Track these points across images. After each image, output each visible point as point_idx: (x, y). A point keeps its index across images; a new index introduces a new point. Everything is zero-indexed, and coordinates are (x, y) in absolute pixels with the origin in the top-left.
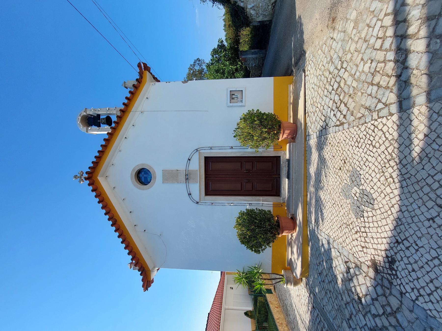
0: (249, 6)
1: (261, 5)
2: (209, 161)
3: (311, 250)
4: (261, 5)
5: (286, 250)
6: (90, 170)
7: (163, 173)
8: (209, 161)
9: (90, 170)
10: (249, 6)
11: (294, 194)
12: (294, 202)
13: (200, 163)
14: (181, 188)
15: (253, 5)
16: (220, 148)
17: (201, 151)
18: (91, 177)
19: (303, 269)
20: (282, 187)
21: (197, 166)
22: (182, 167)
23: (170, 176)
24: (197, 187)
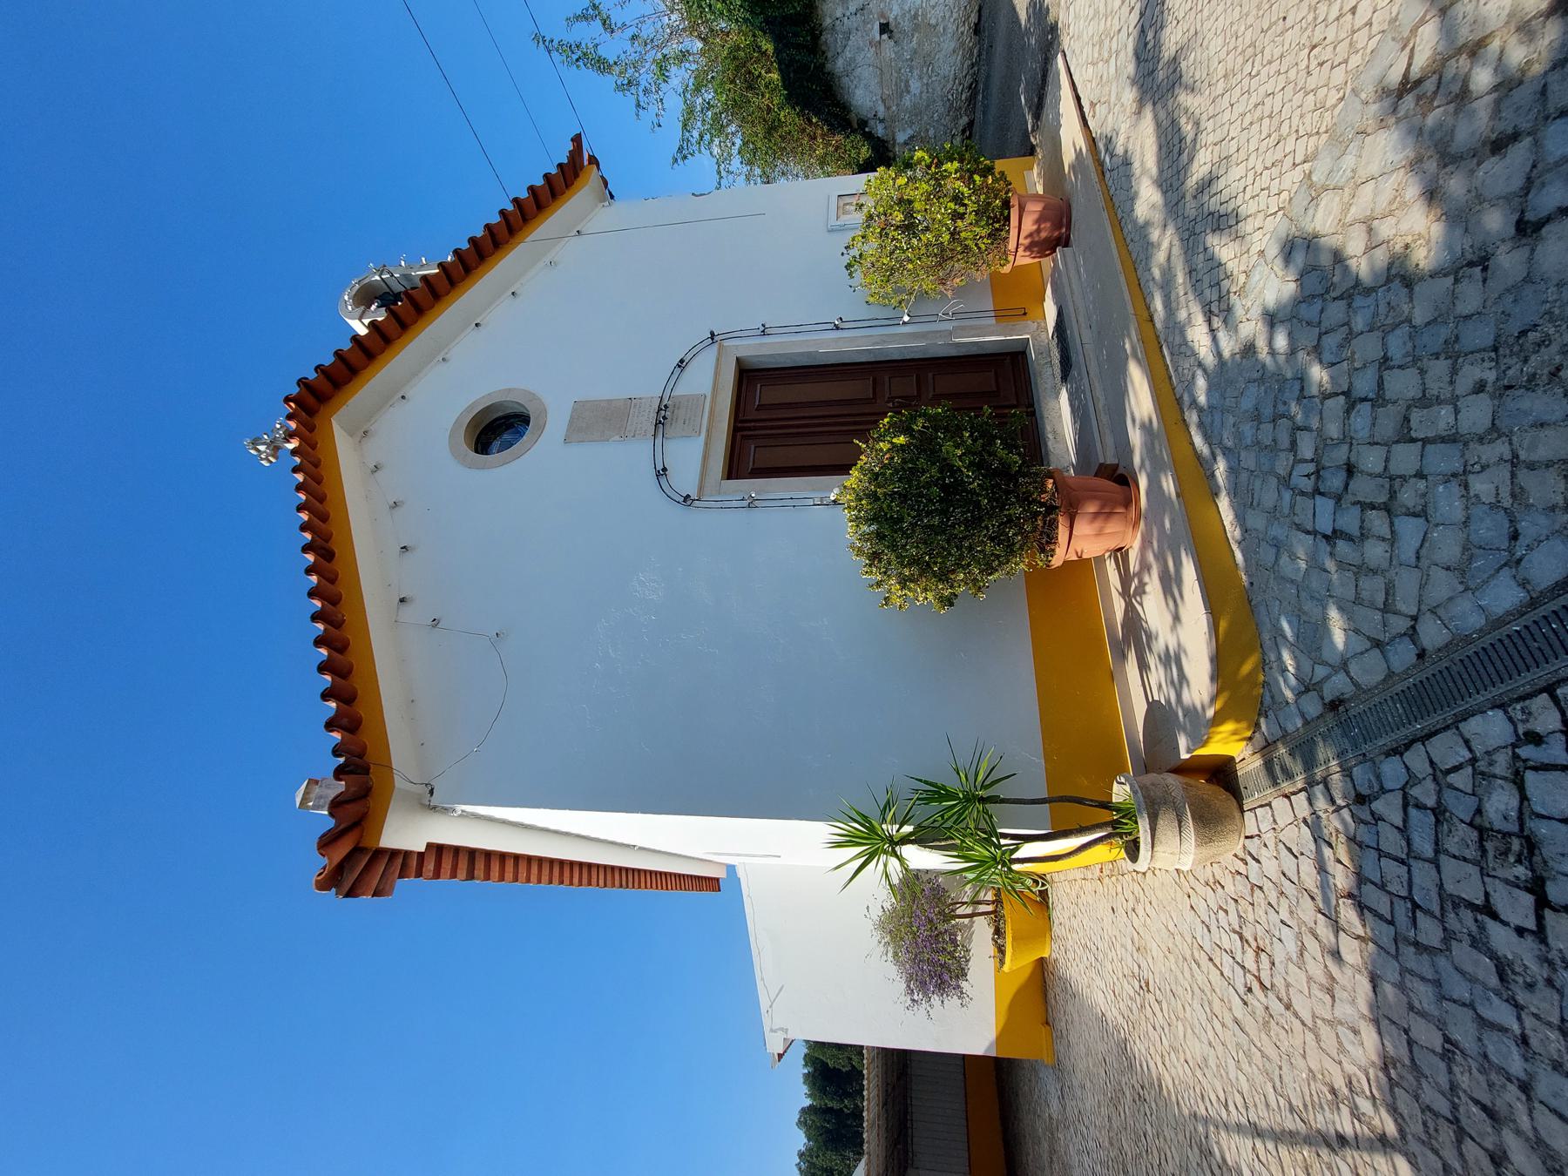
0: (901, 137)
1: (931, 132)
2: (749, 376)
3: (1240, 518)
4: (931, 132)
5: (1114, 677)
6: (342, 760)
7: (574, 410)
8: (749, 376)
9: (342, 760)
10: (901, 137)
11: (1099, 393)
12: (1104, 419)
13: (717, 374)
14: (637, 454)
15: (910, 132)
16: (799, 329)
17: (726, 343)
18: (316, 398)
19: (1223, 625)
20: (1048, 428)
21: (708, 384)
22: (649, 389)
23: (598, 421)
24: (695, 452)
